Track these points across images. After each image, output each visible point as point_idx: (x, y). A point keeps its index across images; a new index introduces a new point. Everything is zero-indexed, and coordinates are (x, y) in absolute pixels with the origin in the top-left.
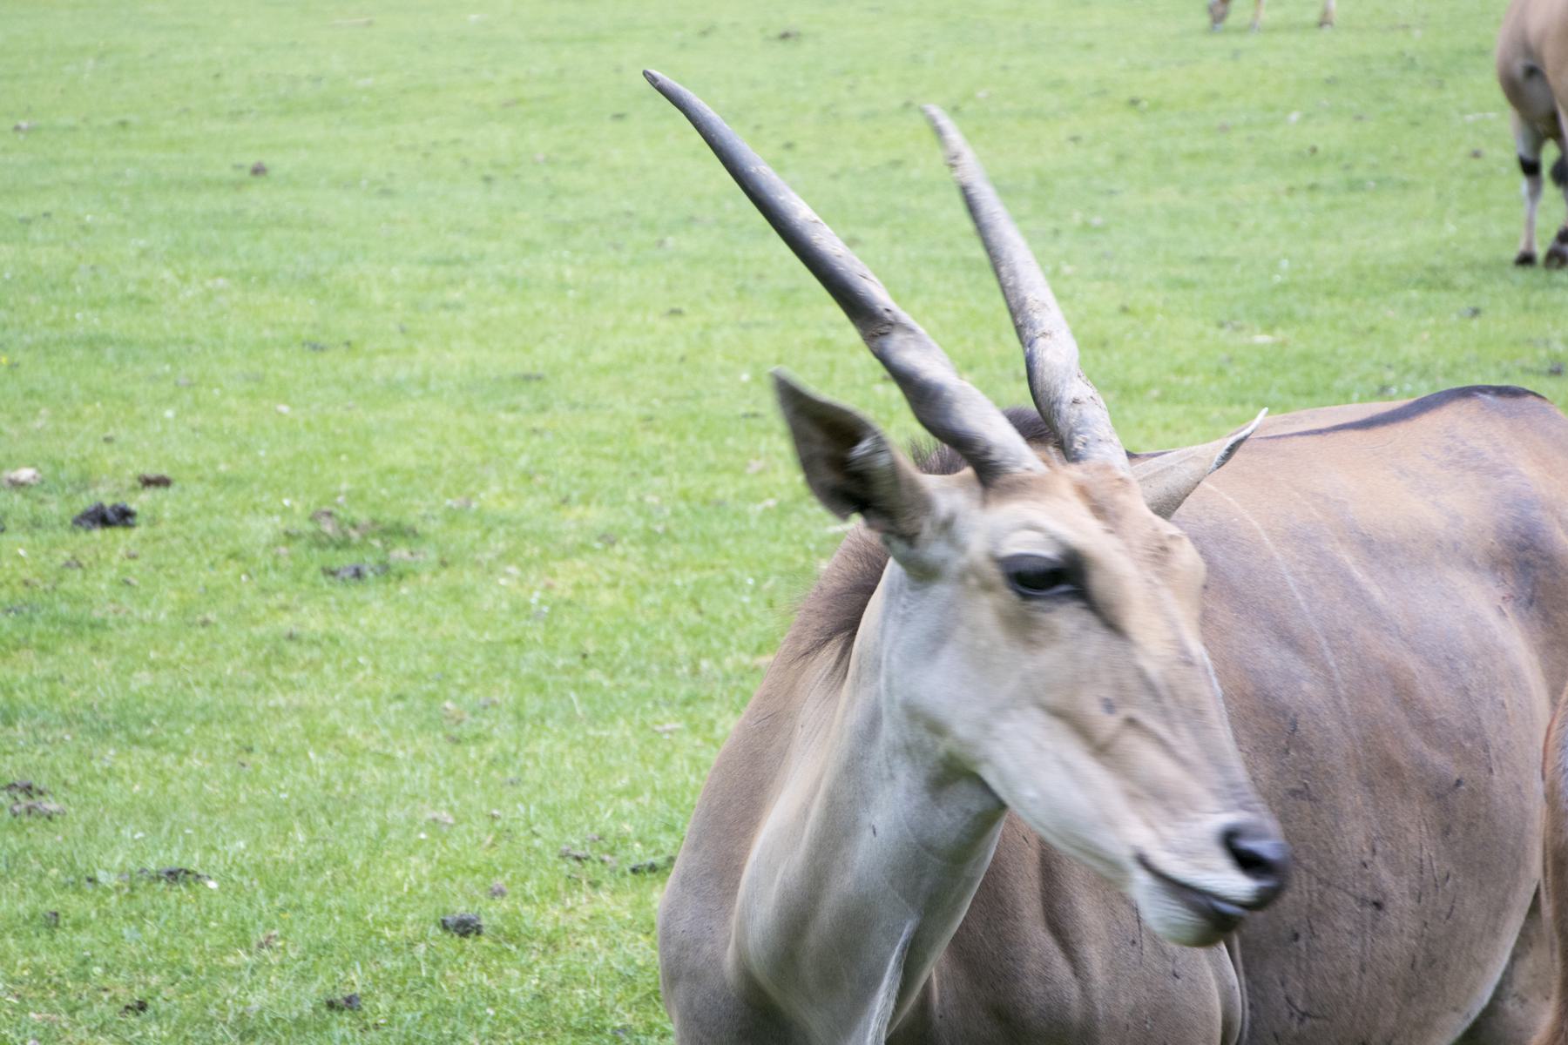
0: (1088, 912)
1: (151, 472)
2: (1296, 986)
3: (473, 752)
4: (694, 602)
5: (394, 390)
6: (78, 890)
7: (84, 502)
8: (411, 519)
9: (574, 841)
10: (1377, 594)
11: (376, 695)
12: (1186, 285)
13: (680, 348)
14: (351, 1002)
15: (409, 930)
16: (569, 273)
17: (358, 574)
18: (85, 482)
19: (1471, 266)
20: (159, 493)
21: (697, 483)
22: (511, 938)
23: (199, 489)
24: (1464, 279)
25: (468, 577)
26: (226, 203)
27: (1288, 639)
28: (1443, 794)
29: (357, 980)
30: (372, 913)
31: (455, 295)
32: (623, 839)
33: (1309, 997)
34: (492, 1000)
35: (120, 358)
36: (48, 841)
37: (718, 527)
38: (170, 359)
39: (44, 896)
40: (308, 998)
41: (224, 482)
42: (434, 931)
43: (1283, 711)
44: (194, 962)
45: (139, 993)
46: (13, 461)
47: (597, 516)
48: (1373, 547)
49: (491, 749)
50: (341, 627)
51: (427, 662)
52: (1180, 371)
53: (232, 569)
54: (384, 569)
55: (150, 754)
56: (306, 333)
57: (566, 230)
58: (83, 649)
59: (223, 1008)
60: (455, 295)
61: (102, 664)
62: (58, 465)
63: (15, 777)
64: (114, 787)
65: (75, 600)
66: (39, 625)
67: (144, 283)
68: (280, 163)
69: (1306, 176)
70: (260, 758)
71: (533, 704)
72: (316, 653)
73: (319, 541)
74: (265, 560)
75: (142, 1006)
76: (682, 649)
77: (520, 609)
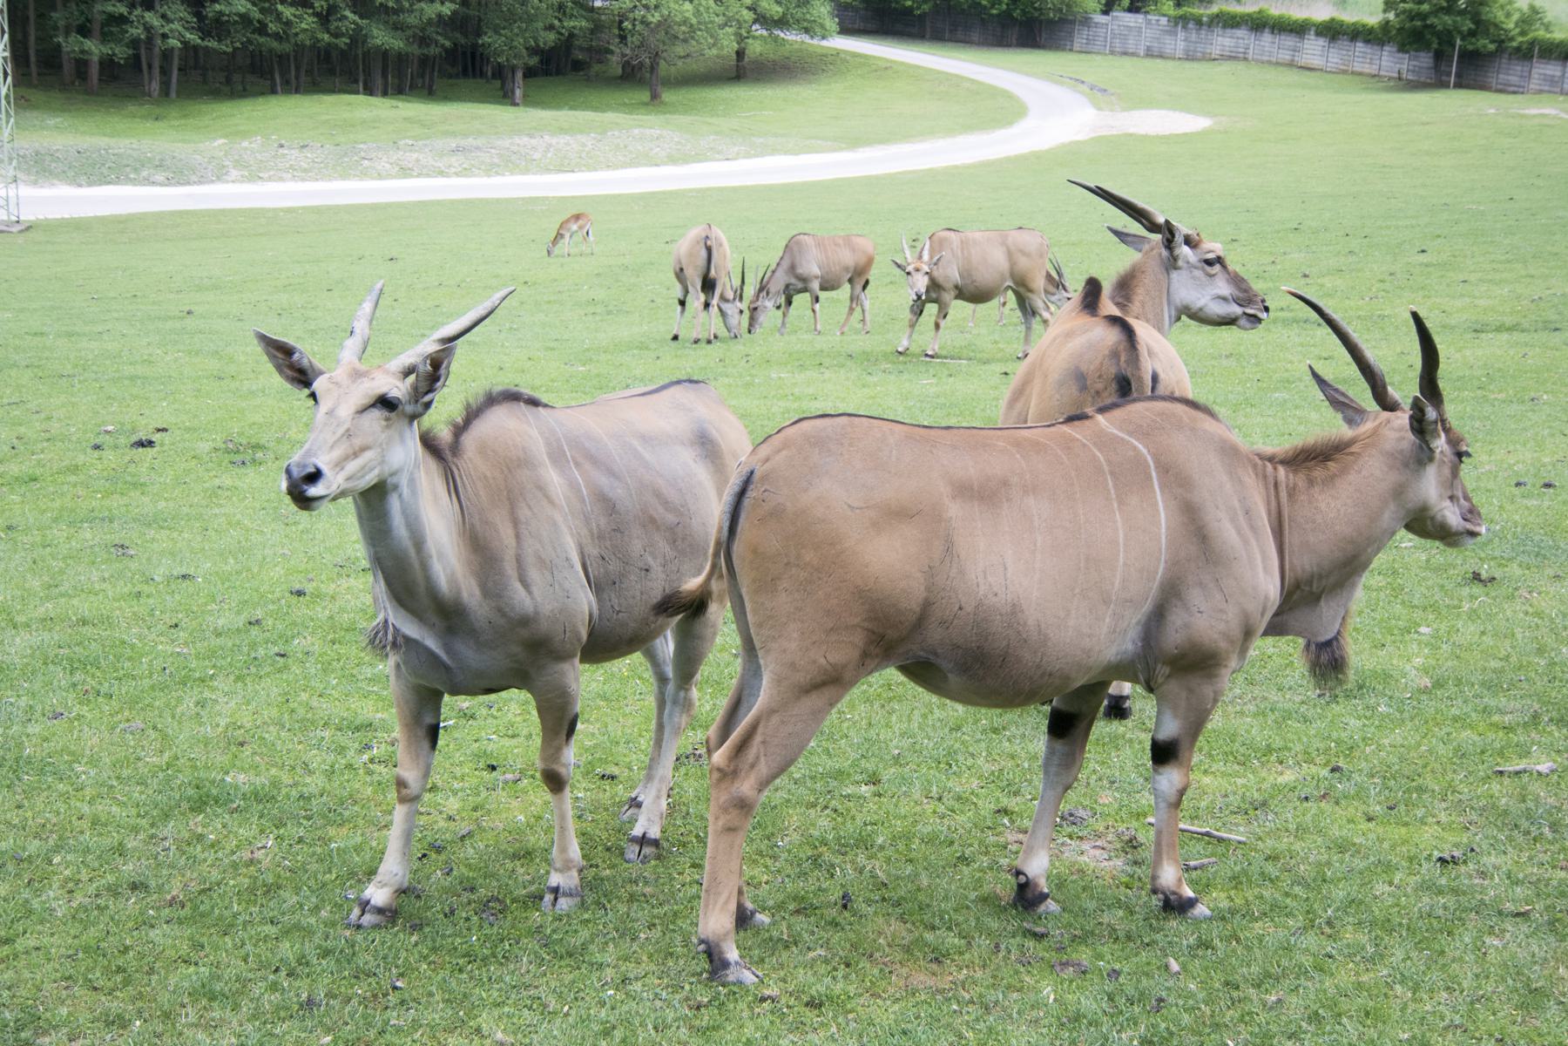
0: (534, 574)
1: (160, 427)
2: (615, 601)
3: (294, 528)
6: (147, 583)
7: (135, 438)
8: (262, 442)
9: (339, 560)
10: (647, 456)
11: (253, 509)
14: (258, 622)
15: (277, 595)
16: (316, 348)
17: (243, 463)
18: (134, 431)
19: (655, 341)
20: (164, 434)
22: (318, 597)
23: (178, 432)
24: (653, 346)
26: (178, 325)
27: (611, 473)
28: (671, 529)
29: (259, 614)
32: (357, 558)
33: (620, 605)
34: (312, 620)
35: (143, 383)
38: (163, 383)
39: (134, 585)
40: (241, 621)
41: (188, 429)
42: (287, 594)
43: (610, 500)
44: (195, 609)
45: (174, 621)
46: (104, 423)
48: (645, 439)
49: (301, 527)
50: (238, 483)
52: (552, 381)
53: (194, 462)
55: (168, 532)
56: (215, 373)
57: (313, 332)
58: (138, 493)
59: (208, 626)
61: (146, 499)
62: (123, 424)
63: (117, 542)
64: (155, 544)
65: (134, 476)
66: (120, 485)
67: (150, 355)
69: (591, 309)
70: (211, 533)
72: (229, 493)
75: (176, 626)
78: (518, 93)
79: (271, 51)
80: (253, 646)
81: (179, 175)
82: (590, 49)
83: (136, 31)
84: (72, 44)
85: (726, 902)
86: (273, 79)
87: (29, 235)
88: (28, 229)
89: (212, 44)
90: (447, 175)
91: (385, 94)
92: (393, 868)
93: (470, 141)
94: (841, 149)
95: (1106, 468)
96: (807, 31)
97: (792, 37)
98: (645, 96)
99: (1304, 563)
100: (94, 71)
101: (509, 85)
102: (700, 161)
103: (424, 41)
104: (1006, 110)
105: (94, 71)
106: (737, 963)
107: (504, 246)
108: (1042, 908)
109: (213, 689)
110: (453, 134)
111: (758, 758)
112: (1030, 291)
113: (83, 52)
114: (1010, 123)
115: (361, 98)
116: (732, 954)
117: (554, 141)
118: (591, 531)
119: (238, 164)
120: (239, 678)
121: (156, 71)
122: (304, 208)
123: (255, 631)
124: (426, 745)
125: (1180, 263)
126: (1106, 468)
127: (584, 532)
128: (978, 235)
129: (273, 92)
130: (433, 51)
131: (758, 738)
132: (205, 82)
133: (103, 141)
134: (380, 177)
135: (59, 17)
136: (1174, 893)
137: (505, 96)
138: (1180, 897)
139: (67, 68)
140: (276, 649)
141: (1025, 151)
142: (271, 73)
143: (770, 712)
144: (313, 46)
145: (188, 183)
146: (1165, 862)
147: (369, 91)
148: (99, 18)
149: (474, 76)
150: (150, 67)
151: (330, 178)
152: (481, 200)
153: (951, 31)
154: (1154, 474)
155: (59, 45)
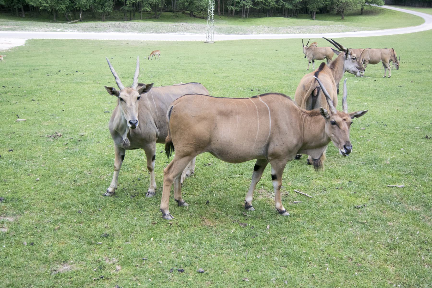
2: (163, 131)
78: (314, 17)
79: (266, 8)
81: (244, 33)
82: (331, 8)
83: (241, 5)
84: (230, 7)
85: (166, 201)
86: (266, 14)
88: (215, 42)
89: (255, 7)
90: (296, 34)
91: (288, 17)
92: (113, 184)
93: (302, 27)
94: (380, 30)
95: (257, 110)
96: (377, 4)
97: (373, 5)
98: (340, 18)
99: (307, 137)
100: (234, 13)
101: (313, 15)
103: (297, 6)
104: (420, 21)
105: (234, 13)
106: (168, 215)
108: (250, 209)
110: (299, 25)
111: (173, 170)
112: (386, 62)
113: (231, 9)
114: (420, 24)
115: (282, 18)
116: (167, 212)
117: (318, 27)
118: (157, 116)
119: (256, 31)
121: (245, 13)
124: (121, 160)
125: (347, 58)
126: (257, 110)
127: (155, 116)
128: (375, 50)
129: (266, 16)
130: (298, 8)
131: (173, 167)
132: (254, 15)
133: (231, 26)
134: (282, 34)
135: (228, 2)
136: (279, 209)
137: (312, 18)
138: (281, 210)
139: (229, 12)
141: (422, 31)
142: (266, 12)
143: (175, 161)
144: (274, 7)
145: (246, 34)
146: (277, 202)
147: (285, 16)
148: (235, 2)
149: (306, 14)
150: (244, 11)
151: (272, 34)
153: (411, 4)
154: (269, 112)
155: (228, 8)
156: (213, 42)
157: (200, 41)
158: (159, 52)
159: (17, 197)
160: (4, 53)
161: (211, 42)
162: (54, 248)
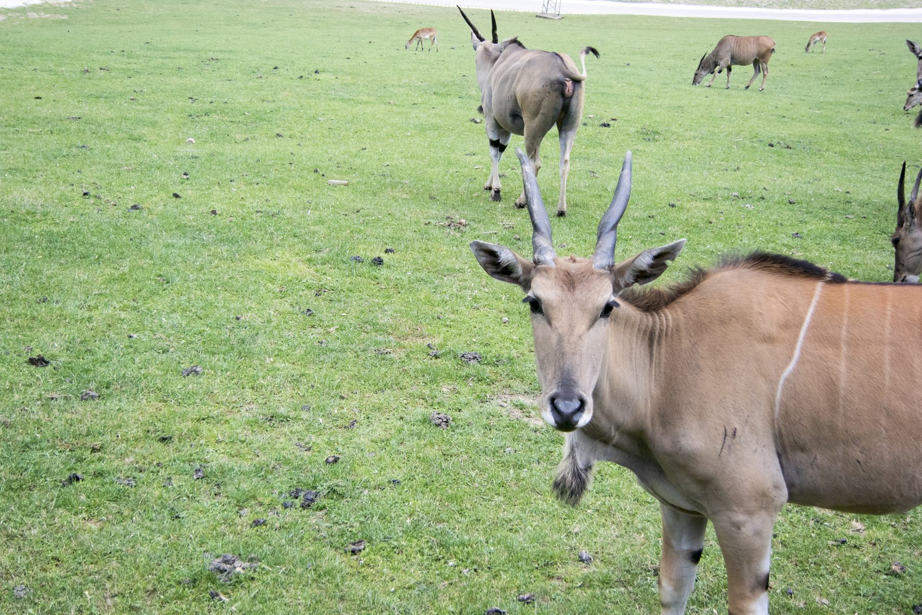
4: (710, 151)
5: (656, 107)
7: (602, 122)
9: (692, 193)
12: (803, 100)
13: (708, 103)
18: (602, 118)
21: (711, 129)
25: (669, 142)
29: (654, 213)
30: (658, 201)
31: (666, 90)
36: (599, 181)
37: (714, 137)
40: (645, 215)
41: (626, 121)
47: (692, 133)
49: (673, 174)
50: (646, 149)
51: (661, 157)
52: (803, 116)
53: (627, 136)
54: (654, 139)
60: (666, 90)
61: (604, 151)
68: (632, 63)
71: (680, 167)
73: (642, 133)
74: (633, 135)
76: (708, 159)
77: (678, 149)
80: (650, 227)
87: (563, 21)
88: (563, 18)
90: (760, 7)
102: (895, 8)
107: (783, 45)
109: (631, 245)
120: (642, 242)
122: (687, 18)
123: (651, 221)
140: (660, 231)
152: (775, 21)
156: (559, 17)
157: (525, 13)
158: (431, 33)
159: (506, 356)
160: (62, 9)
161: (554, 15)
162: (887, 377)
